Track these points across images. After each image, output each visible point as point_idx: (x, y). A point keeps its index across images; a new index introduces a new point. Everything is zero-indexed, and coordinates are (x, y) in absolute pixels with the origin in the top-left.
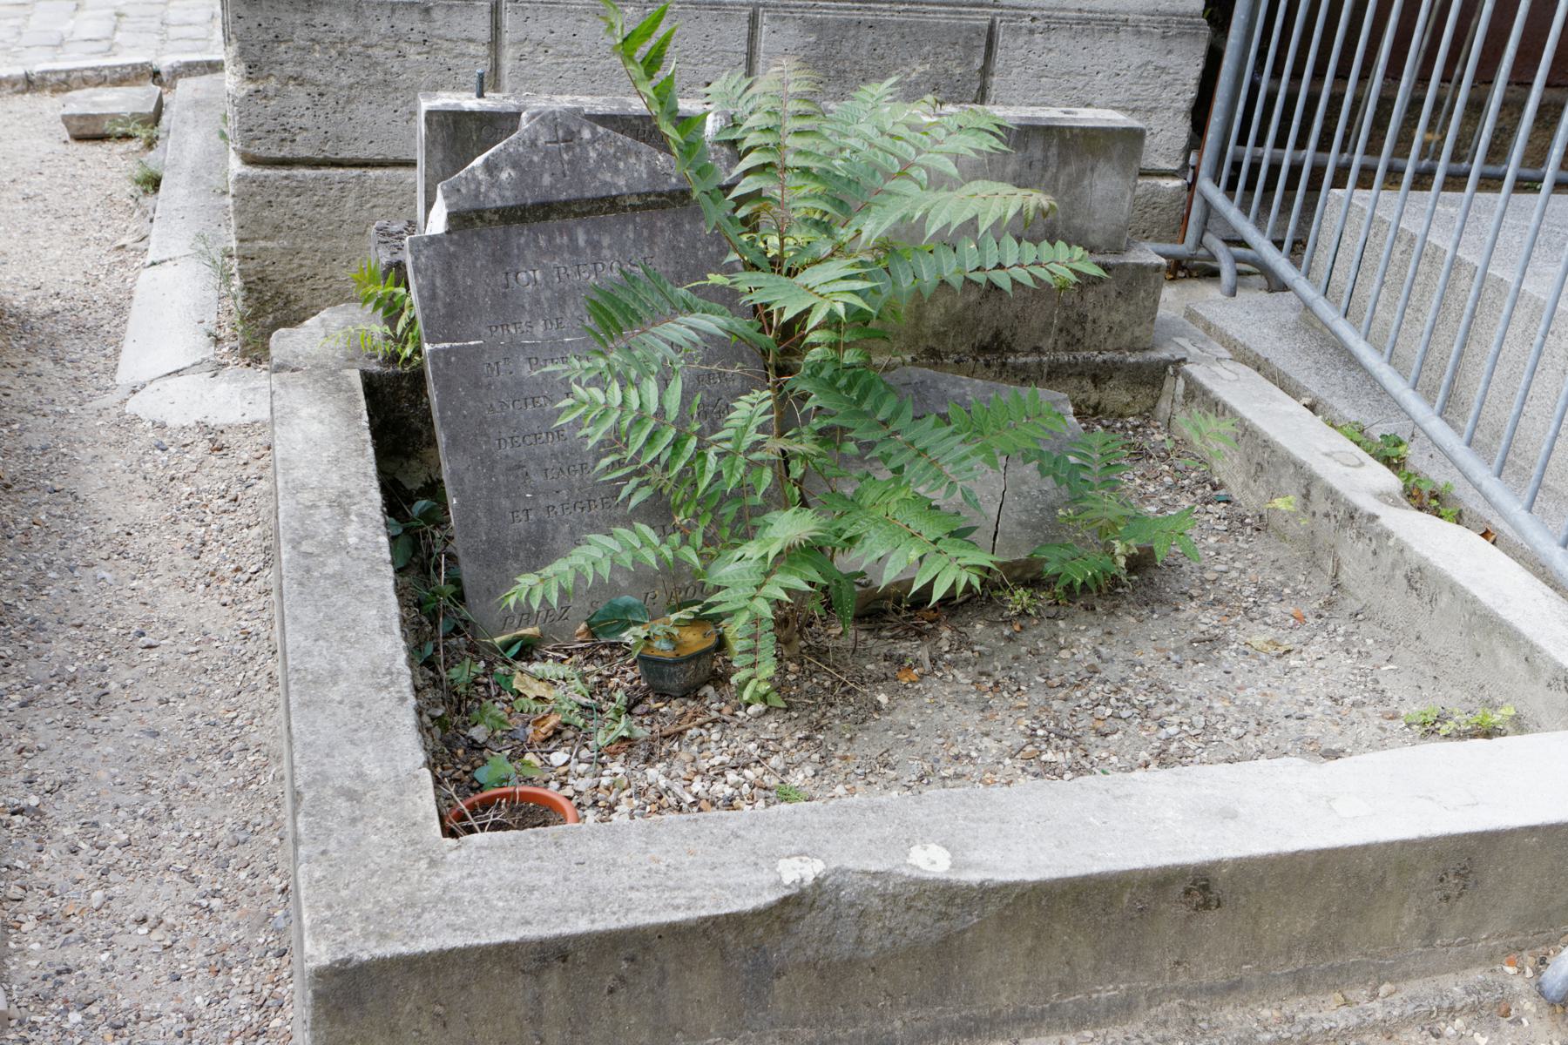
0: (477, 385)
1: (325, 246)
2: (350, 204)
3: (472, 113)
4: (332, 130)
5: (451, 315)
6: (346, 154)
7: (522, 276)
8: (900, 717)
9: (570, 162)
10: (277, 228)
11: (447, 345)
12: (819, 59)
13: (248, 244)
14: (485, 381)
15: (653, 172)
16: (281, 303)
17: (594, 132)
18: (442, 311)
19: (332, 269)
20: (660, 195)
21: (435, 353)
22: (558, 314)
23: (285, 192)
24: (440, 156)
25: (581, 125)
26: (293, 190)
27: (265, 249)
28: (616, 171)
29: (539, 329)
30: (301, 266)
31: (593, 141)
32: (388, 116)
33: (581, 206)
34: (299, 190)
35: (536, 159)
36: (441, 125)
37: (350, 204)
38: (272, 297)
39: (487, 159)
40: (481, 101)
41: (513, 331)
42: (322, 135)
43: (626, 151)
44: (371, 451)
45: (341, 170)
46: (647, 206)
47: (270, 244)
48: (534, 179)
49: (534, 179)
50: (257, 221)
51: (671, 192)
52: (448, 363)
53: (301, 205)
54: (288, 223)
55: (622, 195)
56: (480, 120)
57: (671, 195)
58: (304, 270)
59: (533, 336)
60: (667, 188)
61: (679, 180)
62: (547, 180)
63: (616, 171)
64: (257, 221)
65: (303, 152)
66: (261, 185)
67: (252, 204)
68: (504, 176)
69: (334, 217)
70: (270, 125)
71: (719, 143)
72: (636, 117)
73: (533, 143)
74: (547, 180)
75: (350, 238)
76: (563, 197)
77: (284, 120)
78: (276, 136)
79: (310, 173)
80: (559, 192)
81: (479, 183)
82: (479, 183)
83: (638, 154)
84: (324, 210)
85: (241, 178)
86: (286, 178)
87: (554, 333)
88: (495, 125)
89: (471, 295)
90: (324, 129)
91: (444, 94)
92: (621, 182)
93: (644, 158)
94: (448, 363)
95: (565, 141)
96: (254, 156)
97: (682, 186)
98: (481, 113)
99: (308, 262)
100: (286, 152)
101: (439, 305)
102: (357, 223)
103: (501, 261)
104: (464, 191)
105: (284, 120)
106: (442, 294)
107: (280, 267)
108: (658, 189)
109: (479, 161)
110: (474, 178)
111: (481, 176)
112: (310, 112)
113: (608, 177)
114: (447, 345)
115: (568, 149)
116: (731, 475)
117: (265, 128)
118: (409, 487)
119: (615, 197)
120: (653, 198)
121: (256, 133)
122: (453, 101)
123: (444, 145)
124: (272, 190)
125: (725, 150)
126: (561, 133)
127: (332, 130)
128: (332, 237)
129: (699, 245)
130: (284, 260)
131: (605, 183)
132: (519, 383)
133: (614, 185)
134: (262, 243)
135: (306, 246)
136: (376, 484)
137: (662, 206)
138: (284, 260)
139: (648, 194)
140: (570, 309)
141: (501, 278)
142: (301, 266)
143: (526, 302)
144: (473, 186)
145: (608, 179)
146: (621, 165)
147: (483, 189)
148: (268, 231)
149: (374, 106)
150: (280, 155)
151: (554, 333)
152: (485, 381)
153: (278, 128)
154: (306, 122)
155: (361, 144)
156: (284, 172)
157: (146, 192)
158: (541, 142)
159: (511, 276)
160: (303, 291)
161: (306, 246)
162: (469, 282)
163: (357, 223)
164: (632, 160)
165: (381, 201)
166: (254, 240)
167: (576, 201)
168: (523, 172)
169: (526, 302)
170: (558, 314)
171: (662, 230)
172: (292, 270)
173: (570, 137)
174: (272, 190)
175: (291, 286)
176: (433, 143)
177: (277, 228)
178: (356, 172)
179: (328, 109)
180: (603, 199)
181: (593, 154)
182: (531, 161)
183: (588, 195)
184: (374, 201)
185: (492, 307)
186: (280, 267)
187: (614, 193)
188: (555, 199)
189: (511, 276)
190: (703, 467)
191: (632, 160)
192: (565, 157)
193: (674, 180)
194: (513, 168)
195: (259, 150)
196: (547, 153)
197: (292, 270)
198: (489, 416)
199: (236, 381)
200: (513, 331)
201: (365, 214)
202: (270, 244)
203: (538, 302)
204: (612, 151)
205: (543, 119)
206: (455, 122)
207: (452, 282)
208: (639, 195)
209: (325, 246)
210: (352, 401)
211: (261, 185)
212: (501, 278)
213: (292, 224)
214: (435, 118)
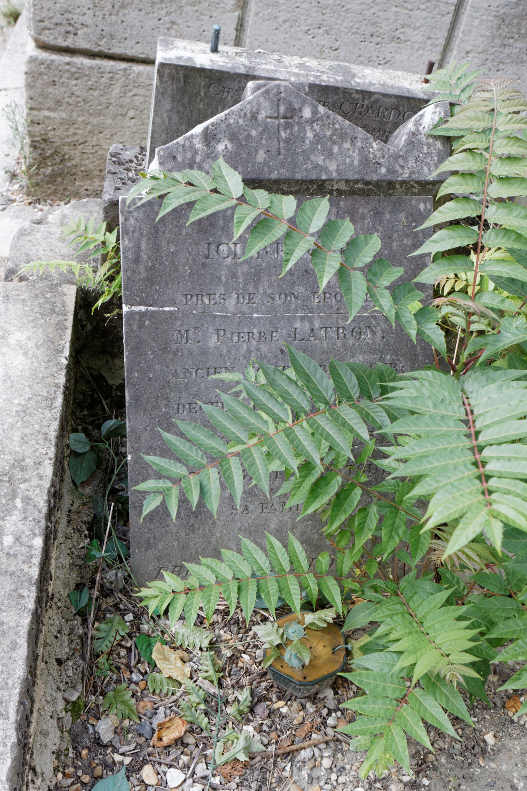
0: (165, 350)
1: (95, 121)
2: (117, 90)
3: (202, 70)
4: (107, 29)
5: (151, 280)
6: (116, 50)
7: (223, 248)
8: (504, 767)
9: (287, 141)
10: (58, 103)
11: (143, 308)
12: (515, 17)
13: (35, 112)
14: (174, 347)
15: (365, 160)
16: (58, 160)
17: (315, 112)
18: (144, 275)
19: (98, 140)
20: (368, 183)
21: (131, 314)
22: (251, 290)
23: (67, 75)
24: (168, 107)
25: (304, 103)
26: (73, 74)
27: (49, 118)
28: (330, 155)
29: (231, 303)
30: (75, 134)
31: (311, 121)
32: (153, 23)
33: (290, 186)
34: (77, 75)
35: (254, 133)
36: (172, 78)
37: (117, 90)
38: (52, 155)
39: (207, 129)
40: (215, 57)
41: (206, 301)
42: (99, 32)
43: (342, 135)
44: (59, 400)
45: (112, 63)
46: (353, 192)
47: (52, 115)
48: (249, 154)
49: (249, 154)
50: (44, 95)
51: (378, 181)
52: (141, 326)
53: (78, 87)
54: (67, 99)
55: (331, 180)
56: (210, 78)
57: (378, 185)
58: (77, 138)
59: (224, 309)
60: (375, 178)
61: (388, 171)
62: (261, 156)
63: (330, 155)
64: (44, 95)
65: (83, 45)
66: (48, 67)
67: (40, 81)
68: (220, 147)
69: (103, 100)
70: (58, 18)
71: (435, 137)
72: (357, 91)
73: (254, 116)
74: (261, 156)
75: (114, 117)
76: (274, 176)
77: (69, 16)
78: (62, 29)
79: (87, 62)
80: (271, 170)
81: (196, 153)
82: (196, 153)
83: (354, 139)
84: (96, 93)
85: (32, 60)
86: (68, 64)
87: (245, 308)
88: (221, 86)
89: (173, 262)
90: (101, 27)
91: (180, 43)
92: (333, 166)
93: (359, 144)
94: (141, 326)
95: (285, 117)
96: (44, 43)
97: (390, 177)
98: (211, 71)
99: (80, 132)
100: (69, 43)
101: (142, 269)
102: (121, 106)
103: (206, 232)
104: (179, 158)
105: (69, 16)
106: (145, 257)
107: (59, 133)
108: (367, 178)
109: (198, 129)
110: (192, 147)
111: (198, 145)
112: (90, 12)
113: (320, 160)
114: (143, 308)
115: (287, 126)
116: (390, 537)
117: (54, 20)
118: (111, 382)
119: (324, 181)
120: (360, 186)
121: (46, 24)
122: (186, 54)
123: (173, 97)
124: (57, 72)
125: (439, 144)
126: (282, 109)
127: (107, 29)
128: (100, 114)
129: (395, 236)
130: (62, 128)
131: (316, 166)
132: (205, 353)
133: (325, 169)
134: (46, 113)
135: (80, 119)
136: (52, 452)
137: (366, 193)
138: (62, 128)
139: (356, 182)
140: (264, 287)
141: (203, 248)
142: (75, 134)
143: (224, 274)
144: (189, 155)
145: (321, 162)
146: (336, 149)
147: (198, 159)
148: (51, 104)
149: (142, 13)
150: (64, 44)
151: (245, 308)
152: (174, 347)
153: (65, 22)
154: (88, 19)
155: (130, 43)
156: (67, 59)
157: (9, 23)
158: (261, 116)
159: (213, 247)
160: (76, 153)
161: (80, 119)
162: (172, 249)
163: (121, 106)
164: (347, 145)
165: (141, 91)
166: (40, 109)
167: (286, 181)
168: (239, 146)
169: (224, 274)
170: (251, 290)
171: (363, 218)
172: (68, 136)
173: (291, 114)
174: (57, 72)
175: (66, 149)
176: (163, 94)
177: (58, 103)
178: (123, 65)
179: (106, 11)
180: (312, 182)
181: (310, 135)
182: (249, 135)
183: (298, 176)
184: (135, 91)
185: (191, 275)
186: (59, 133)
187: (324, 177)
188: (266, 176)
189: (213, 247)
190: (362, 524)
191: (347, 145)
192: (283, 134)
193: (383, 170)
194: (231, 140)
195: (48, 38)
196: (266, 128)
197: (68, 136)
198: (173, 381)
199: (18, 217)
200: (206, 301)
201: (127, 100)
202: (52, 115)
203: (234, 275)
204: (329, 133)
205: (267, 92)
206: (186, 77)
207: (156, 248)
208: (347, 181)
209: (95, 121)
210: (60, 327)
211: (48, 67)
212: (203, 248)
213: (71, 101)
214: (167, 71)
